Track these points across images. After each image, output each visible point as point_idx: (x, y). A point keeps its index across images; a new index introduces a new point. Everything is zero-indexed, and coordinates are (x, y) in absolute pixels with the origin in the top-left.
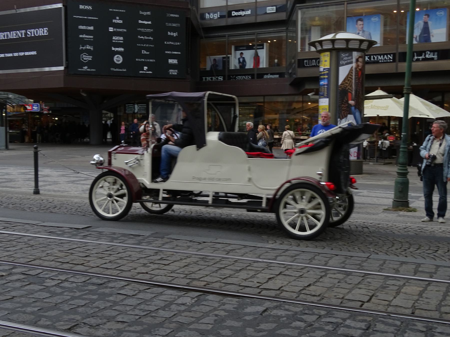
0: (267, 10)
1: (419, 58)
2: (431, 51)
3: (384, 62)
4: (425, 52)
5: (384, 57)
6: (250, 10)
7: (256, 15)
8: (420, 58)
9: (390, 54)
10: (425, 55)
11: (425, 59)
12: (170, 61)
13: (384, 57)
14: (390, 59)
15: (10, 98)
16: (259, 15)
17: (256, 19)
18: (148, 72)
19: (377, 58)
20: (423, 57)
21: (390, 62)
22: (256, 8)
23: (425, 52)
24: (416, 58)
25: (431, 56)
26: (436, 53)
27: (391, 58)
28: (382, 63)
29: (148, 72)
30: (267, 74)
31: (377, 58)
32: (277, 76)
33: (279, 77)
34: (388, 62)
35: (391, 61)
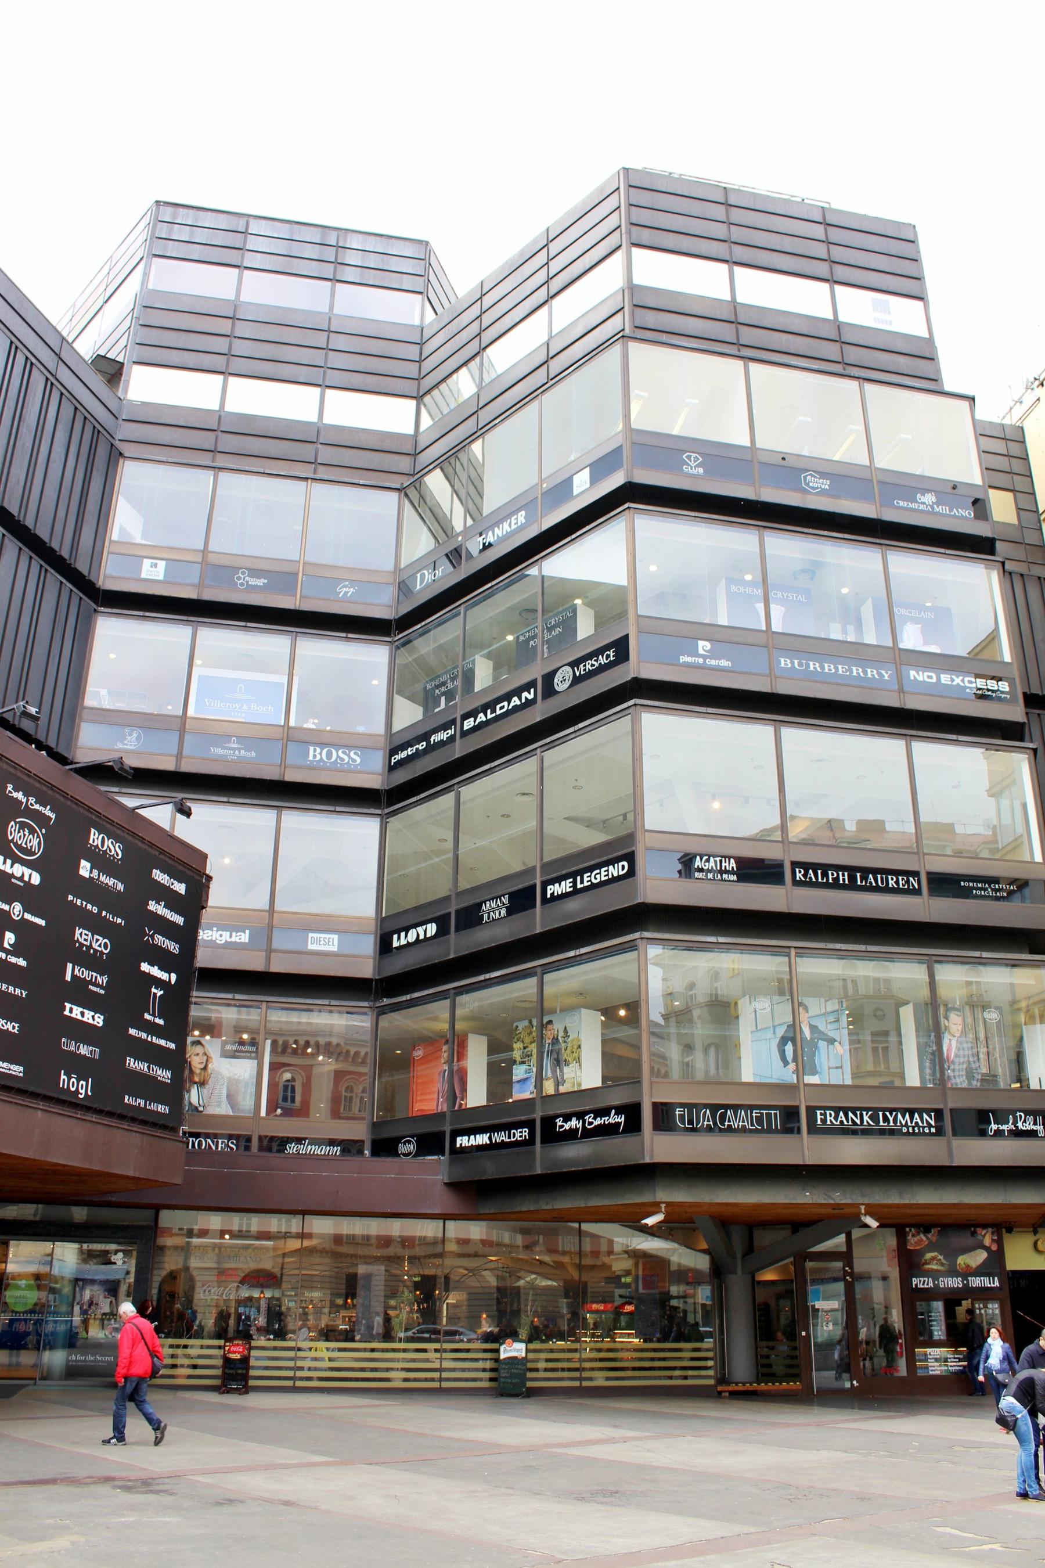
0: (336, 942)
1: (1001, 1128)
2: (1027, 1113)
3: (914, 1134)
4: (1013, 1112)
5: (912, 1118)
6: (247, 932)
7: (270, 951)
8: (1005, 1127)
9: (928, 1111)
10: (1015, 1123)
11: (1018, 1134)
12: (74, 1012)
13: (912, 1118)
14: (930, 1126)
15: (1028, 1006)
16: (277, 951)
17: (268, 960)
18: (13, 960)
19: (895, 1120)
20: (1011, 1126)
21: (930, 1134)
22: (271, 927)
23: (1013, 1112)
24: (994, 1127)
25: (1029, 1126)
26: (1040, 1119)
27: (933, 1123)
28: (908, 1134)
29: (13, 960)
30: (299, 1141)
31: (895, 1120)
32: (337, 1150)
33: (343, 1151)
34: (924, 1134)
35: (933, 1130)
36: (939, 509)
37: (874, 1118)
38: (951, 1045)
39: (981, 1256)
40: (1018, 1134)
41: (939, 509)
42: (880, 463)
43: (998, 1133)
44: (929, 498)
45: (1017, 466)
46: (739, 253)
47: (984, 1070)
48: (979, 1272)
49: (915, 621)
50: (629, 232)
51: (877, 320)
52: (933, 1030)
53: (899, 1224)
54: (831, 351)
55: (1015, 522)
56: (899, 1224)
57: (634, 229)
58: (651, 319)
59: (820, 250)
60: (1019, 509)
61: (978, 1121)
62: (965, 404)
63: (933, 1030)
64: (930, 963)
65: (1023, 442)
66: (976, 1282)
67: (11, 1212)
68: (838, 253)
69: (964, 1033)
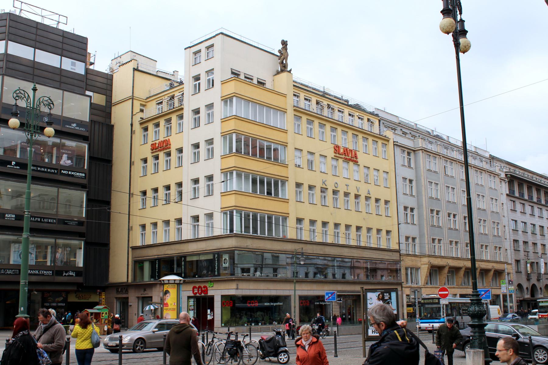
25: (72, 274)
36: (76, 128)
37: (39, 272)
38: (58, 255)
39: (62, 298)
40: (69, 276)
41: (76, 128)
42: (64, 115)
43: (65, 275)
44: (74, 125)
45: (109, 87)
46: (38, 45)
47: (65, 260)
48: (60, 302)
49: (66, 154)
50: (8, 36)
51: (72, 69)
52: (54, 253)
53: (43, 292)
54: (57, 78)
55: (104, 105)
56: (43, 292)
57: (10, 35)
58: (11, 65)
59: (60, 45)
60: (106, 101)
61: (59, 273)
62: (89, 98)
63: (54, 253)
64: (56, 239)
65: (112, 80)
66: (60, 304)
67: (64, 361)
68: (65, 47)
69: (62, 253)
